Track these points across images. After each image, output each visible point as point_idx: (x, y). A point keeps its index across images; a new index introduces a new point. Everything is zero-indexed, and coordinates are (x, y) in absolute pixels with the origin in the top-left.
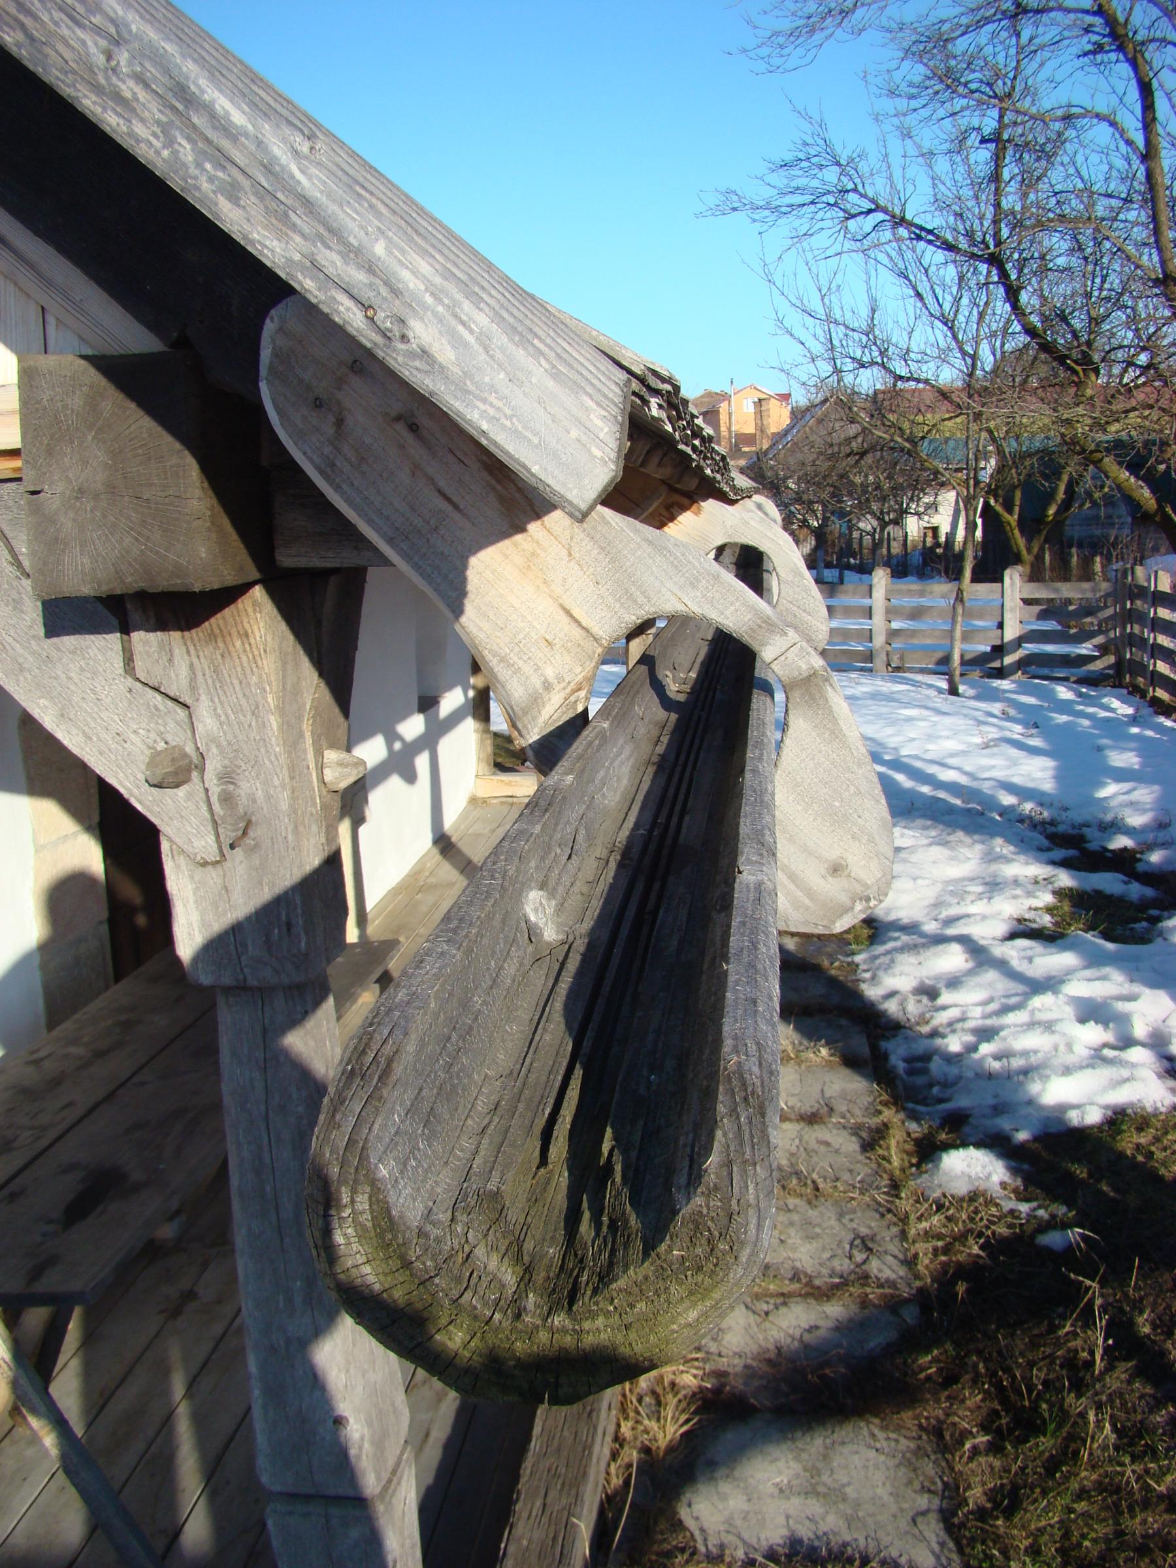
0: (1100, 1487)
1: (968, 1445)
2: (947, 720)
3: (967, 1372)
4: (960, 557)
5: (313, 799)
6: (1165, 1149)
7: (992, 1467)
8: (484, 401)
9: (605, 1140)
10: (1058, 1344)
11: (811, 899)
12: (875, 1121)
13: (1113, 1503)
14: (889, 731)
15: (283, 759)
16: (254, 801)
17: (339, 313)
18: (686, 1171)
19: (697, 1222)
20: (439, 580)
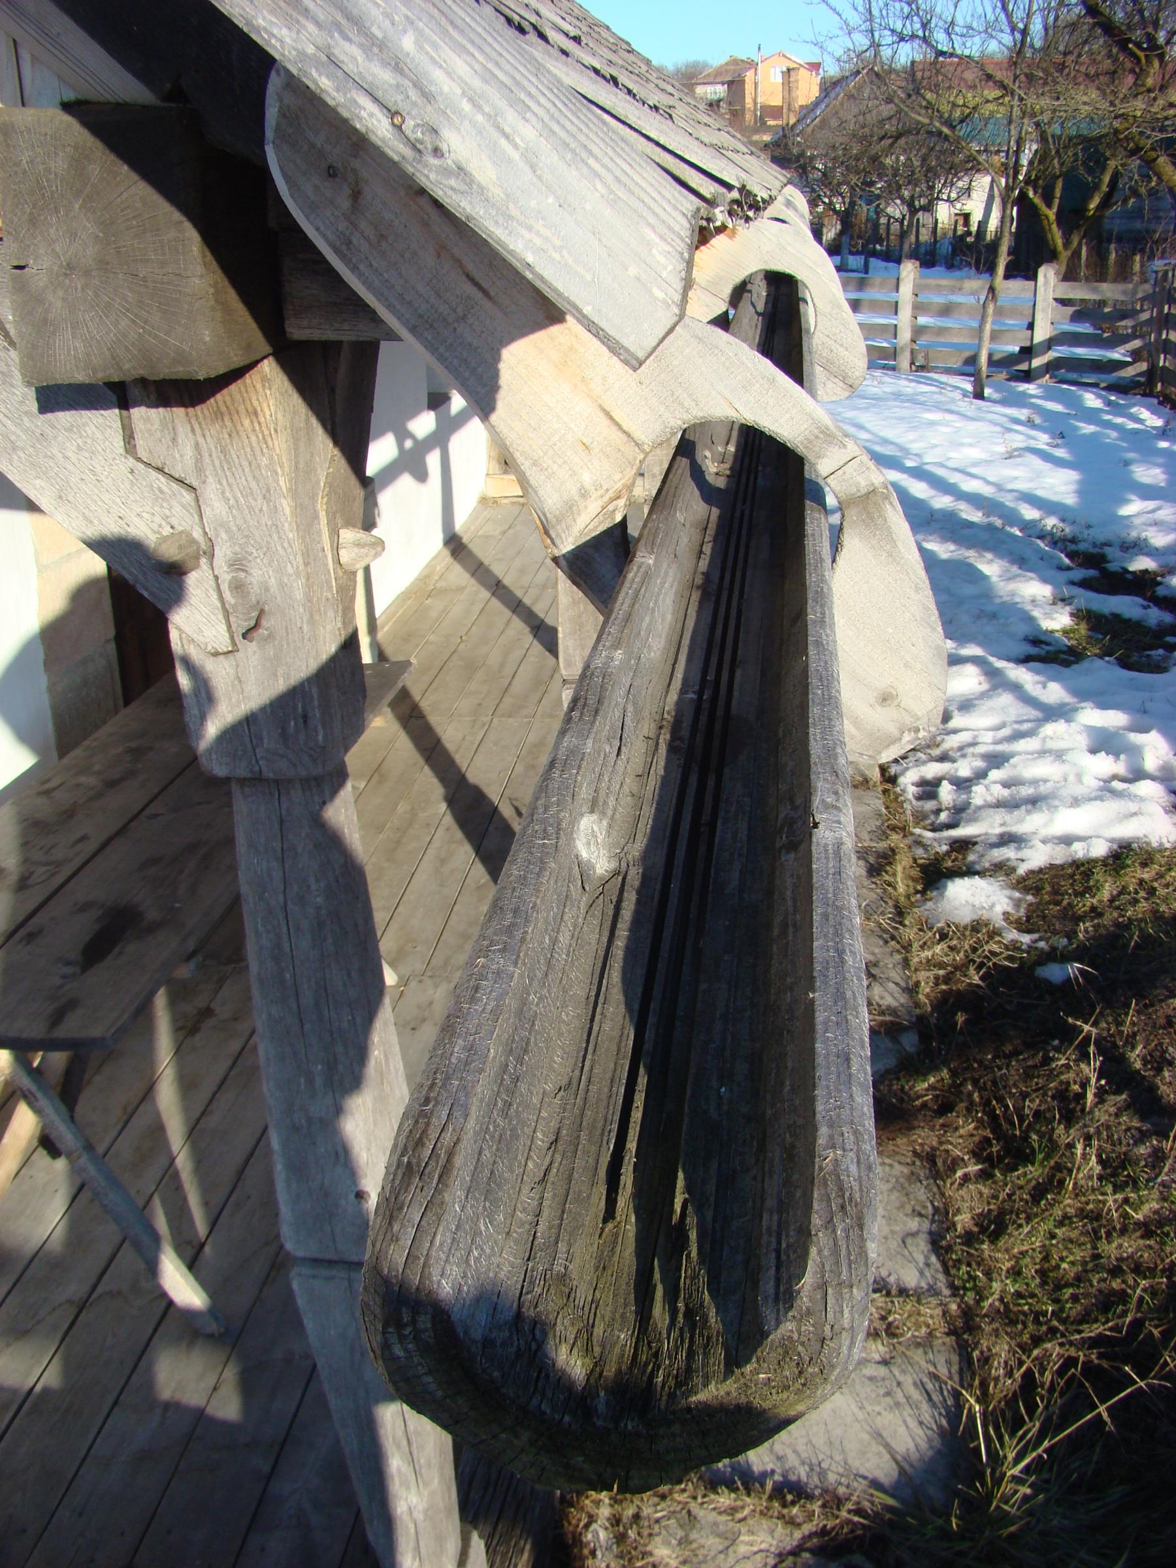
0: (1082, 1214)
1: (959, 1173)
2: (972, 426)
3: (962, 1101)
4: (994, 247)
5: (329, 582)
6: (1167, 886)
7: (981, 1194)
8: (529, 229)
9: (677, 1194)
10: (1051, 1076)
11: (858, 729)
12: (882, 845)
13: (1093, 1229)
14: (911, 436)
15: (297, 546)
16: (267, 589)
17: (360, 119)
18: (772, 1271)
19: (787, 1347)
20: (467, 374)
